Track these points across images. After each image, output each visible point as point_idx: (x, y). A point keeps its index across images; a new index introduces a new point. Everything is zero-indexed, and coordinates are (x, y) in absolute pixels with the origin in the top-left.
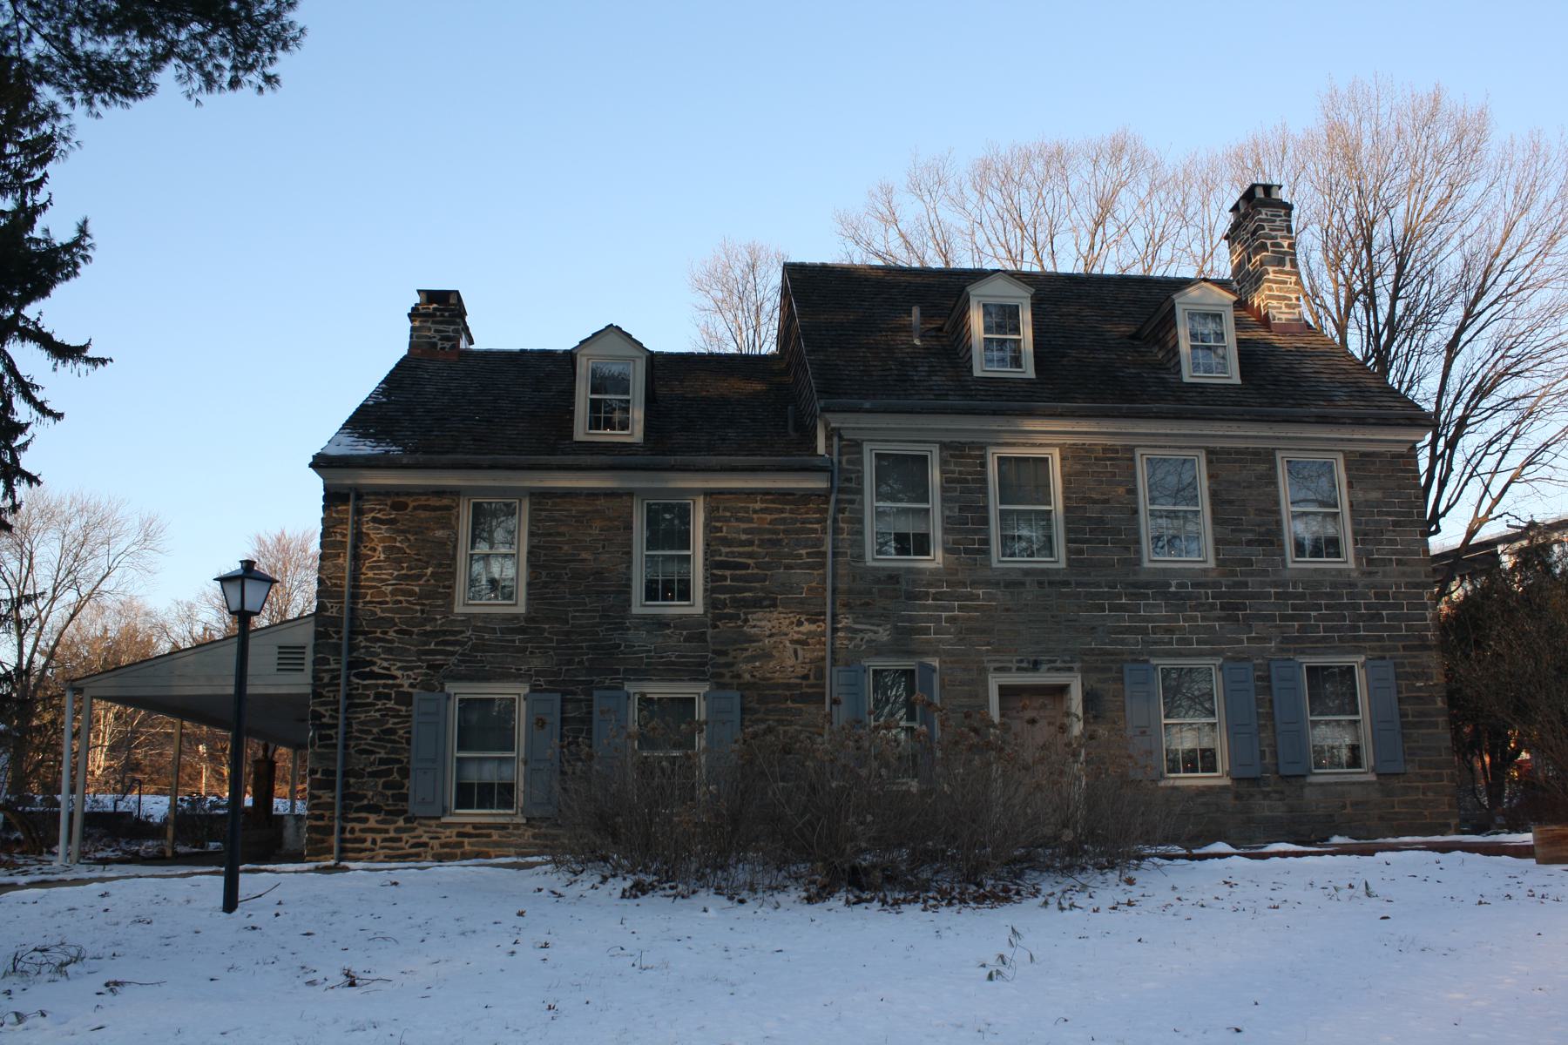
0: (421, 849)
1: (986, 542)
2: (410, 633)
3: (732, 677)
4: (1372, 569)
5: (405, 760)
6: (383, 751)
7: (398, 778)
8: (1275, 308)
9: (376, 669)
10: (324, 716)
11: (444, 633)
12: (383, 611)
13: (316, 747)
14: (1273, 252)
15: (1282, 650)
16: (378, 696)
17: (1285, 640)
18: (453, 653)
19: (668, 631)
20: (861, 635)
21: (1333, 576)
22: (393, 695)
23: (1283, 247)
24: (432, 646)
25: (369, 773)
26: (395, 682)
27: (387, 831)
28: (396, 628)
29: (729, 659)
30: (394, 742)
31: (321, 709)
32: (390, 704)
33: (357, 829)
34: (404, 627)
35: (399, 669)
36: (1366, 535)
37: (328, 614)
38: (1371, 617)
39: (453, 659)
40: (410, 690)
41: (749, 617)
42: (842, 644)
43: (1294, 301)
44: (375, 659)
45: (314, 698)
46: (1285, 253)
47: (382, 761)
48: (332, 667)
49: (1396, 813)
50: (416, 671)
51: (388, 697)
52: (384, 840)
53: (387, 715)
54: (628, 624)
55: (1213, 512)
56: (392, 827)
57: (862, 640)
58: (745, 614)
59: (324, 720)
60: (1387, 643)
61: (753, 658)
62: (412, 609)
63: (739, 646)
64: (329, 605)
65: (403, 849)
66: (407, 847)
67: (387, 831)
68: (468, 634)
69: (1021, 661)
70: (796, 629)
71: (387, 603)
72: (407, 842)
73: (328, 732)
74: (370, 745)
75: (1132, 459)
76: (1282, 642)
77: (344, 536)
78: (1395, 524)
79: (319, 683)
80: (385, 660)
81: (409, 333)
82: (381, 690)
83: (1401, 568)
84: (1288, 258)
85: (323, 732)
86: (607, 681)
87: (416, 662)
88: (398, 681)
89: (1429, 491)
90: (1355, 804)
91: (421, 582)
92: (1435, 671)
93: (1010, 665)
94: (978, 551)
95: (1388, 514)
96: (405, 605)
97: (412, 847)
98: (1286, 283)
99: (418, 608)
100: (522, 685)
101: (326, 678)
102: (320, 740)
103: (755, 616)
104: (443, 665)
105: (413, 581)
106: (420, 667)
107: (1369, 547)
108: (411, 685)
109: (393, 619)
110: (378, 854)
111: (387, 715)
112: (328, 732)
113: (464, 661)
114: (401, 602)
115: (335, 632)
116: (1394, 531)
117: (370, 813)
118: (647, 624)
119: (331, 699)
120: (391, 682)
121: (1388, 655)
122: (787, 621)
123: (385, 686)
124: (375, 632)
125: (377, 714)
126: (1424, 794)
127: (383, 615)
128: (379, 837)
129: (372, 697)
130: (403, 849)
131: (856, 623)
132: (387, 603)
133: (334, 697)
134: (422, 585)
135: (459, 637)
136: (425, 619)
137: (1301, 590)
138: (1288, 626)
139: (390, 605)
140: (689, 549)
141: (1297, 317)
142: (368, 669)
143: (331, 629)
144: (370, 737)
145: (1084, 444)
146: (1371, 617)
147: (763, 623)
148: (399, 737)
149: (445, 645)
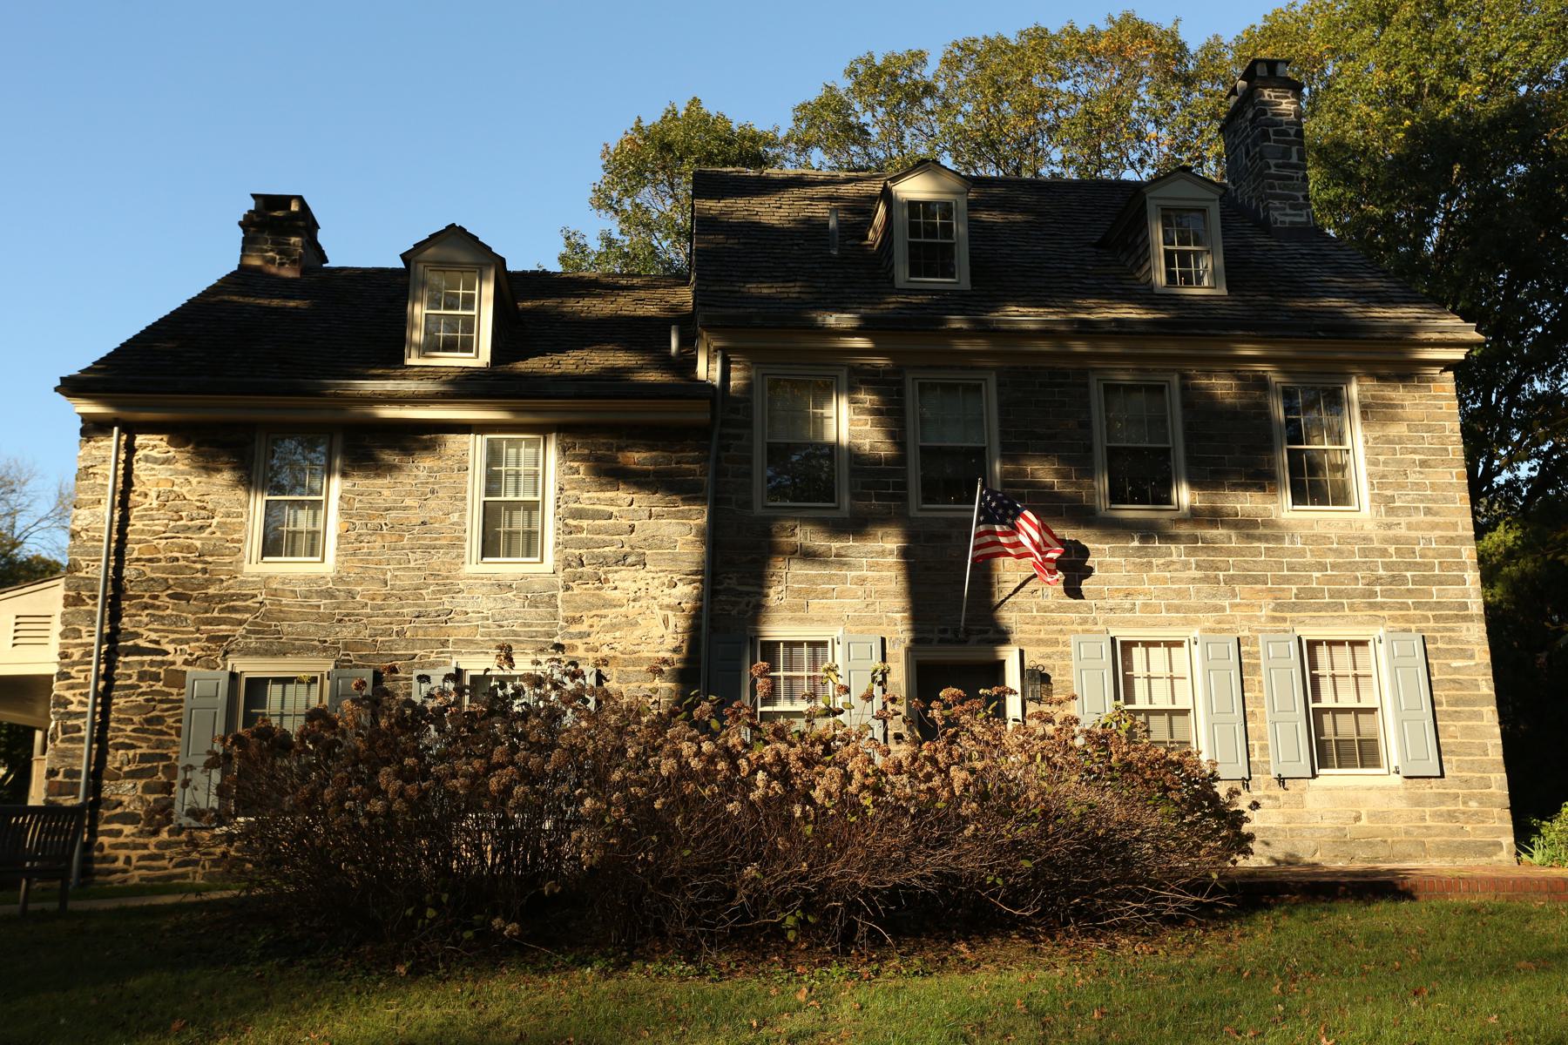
0: (190, 868)
1: (903, 486)
2: (188, 598)
3: (587, 650)
4: (1394, 520)
5: (174, 756)
6: (144, 745)
7: (164, 779)
8: (1277, 209)
9: (142, 643)
10: (72, 703)
11: (231, 597)
12: (153, 570)
13: (58, 742)
14: (1275, 141)
15: (1274, 619)
16: (142, 676)
17: (1279, 607)
18: (241, 623)
19: (510, 595)
20: (746, 599)
21: (1342, 528)
22: (162, 676)
23: (1289, 135)
24: (216, 614)
25: (126, 773)
26: (165, 658)
27: (145, 846)
28: (169, 592)
29: (584, 628)
30: (161, 733)
31: (68, 694)
32: (159, 686)
33: (106, 845)
34: (180, 590)
35: (173, 641)
36: (1384, 477)
37: (83, 574)
38: (1393, 580)
39: (241, 630)
40: (185, 668)
41: (610, 576)
42: (723, 609)
43: (1301, 200)
44: (140, 630)
45: (59, 680)
46: (1291, 143)
47: (144, 758)
48: (84, 641)
49: (1427, 828)
50: (192, 644)
51: (156, 677)
52: (142, 858)
53: (153, 700)
54: (461, 586)
55: (1187, 448)
56: (153, 840)
57: (747, 605)
58: (605, 573)
59: (72, 708)
60: (1412, 612)
61: (614, 627)
62: (191, 568)
63: (598, 612)
64: (84, 564)
65: (166, 868)
66: (170, 866)
67: (145, 846)
68: (260, 599)
69: (945, 631)
70: (667, 591)
71: (159, 560)
72: (171, 859)
73: (75, 722)
74: (128, 737)
75: (1086, 385)
76: (1274, 610)
77: (106, 477)
78: (1423, 464)
79: (67, 660)
80: (156, 631)
81: (240, 245)
82: (146, 668)
83: (1429, 518)
84: (1294, 149)
85: (69, 723)
86: (433, 655)
87: (192, 633)
88: (169, 658)
89: (580, 345)
90: (1373, 816)
91: (203, 535)
92: (1477, 648)
93: (931, 636)
94: (893, 497)
95: (1414, 451)
96: (182, 563)
97: (176, 866)
98: (1291, 178)
99: (199, 566)
100: (327, 661)
101: (77, 654)
102: (64, 733)
103: (617, 576)
104: (228, 636)
105: (194, 532)
106: (198, 640)
107: (1389, 493)
108: (186, 662)
109: (166, 580)
110: (133, 876)
111: (153, 700)
112: (75, 722)
113: (255, 632)
114: (177, 559)
115: (89, 597)
116: (1421, 473)
117: (125, 823)
118: (484, 585)
119: (82, 681)
120: (159, 658)
121: (1413, 627)
122: (656, 582)
123: (152, 663)
124: (143, 597)
125: (141, 699)
126: (1465, 803)
127: (153, 575)
128: (134, 854)
129: (135, 677)
130: (166, 868)
131: (740, 584)
132: (159, 560)
133: (86, 678)
134: (205, 539)
135: (249, 603)
136: (207, 580)
137: (1299, 546)
138: (1284, 590)
139: (163, 563)
140: (473, 309)
141: (1304, 219)
142: (130, 643)
143: (84, 593)
144: (130, 728)
145: (1026, 368)
146: (1393, 580)
147: (626, 585)
148: (168, 727)
149: (229, 612)
